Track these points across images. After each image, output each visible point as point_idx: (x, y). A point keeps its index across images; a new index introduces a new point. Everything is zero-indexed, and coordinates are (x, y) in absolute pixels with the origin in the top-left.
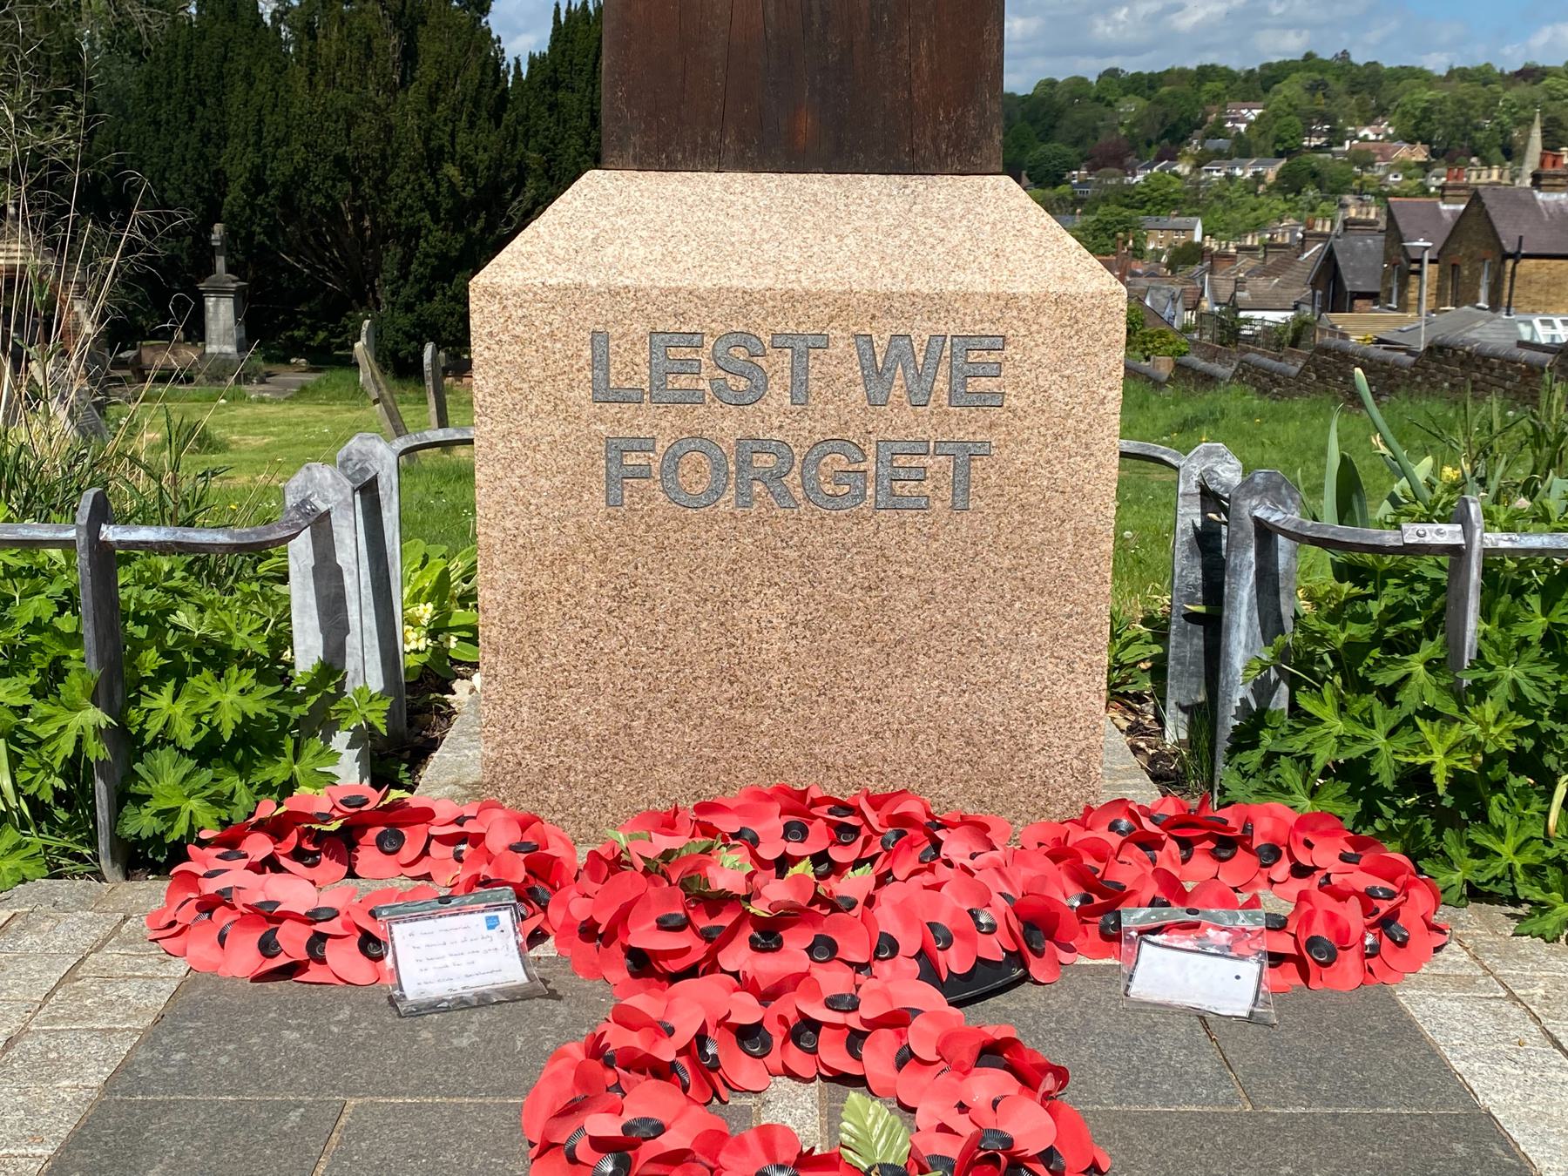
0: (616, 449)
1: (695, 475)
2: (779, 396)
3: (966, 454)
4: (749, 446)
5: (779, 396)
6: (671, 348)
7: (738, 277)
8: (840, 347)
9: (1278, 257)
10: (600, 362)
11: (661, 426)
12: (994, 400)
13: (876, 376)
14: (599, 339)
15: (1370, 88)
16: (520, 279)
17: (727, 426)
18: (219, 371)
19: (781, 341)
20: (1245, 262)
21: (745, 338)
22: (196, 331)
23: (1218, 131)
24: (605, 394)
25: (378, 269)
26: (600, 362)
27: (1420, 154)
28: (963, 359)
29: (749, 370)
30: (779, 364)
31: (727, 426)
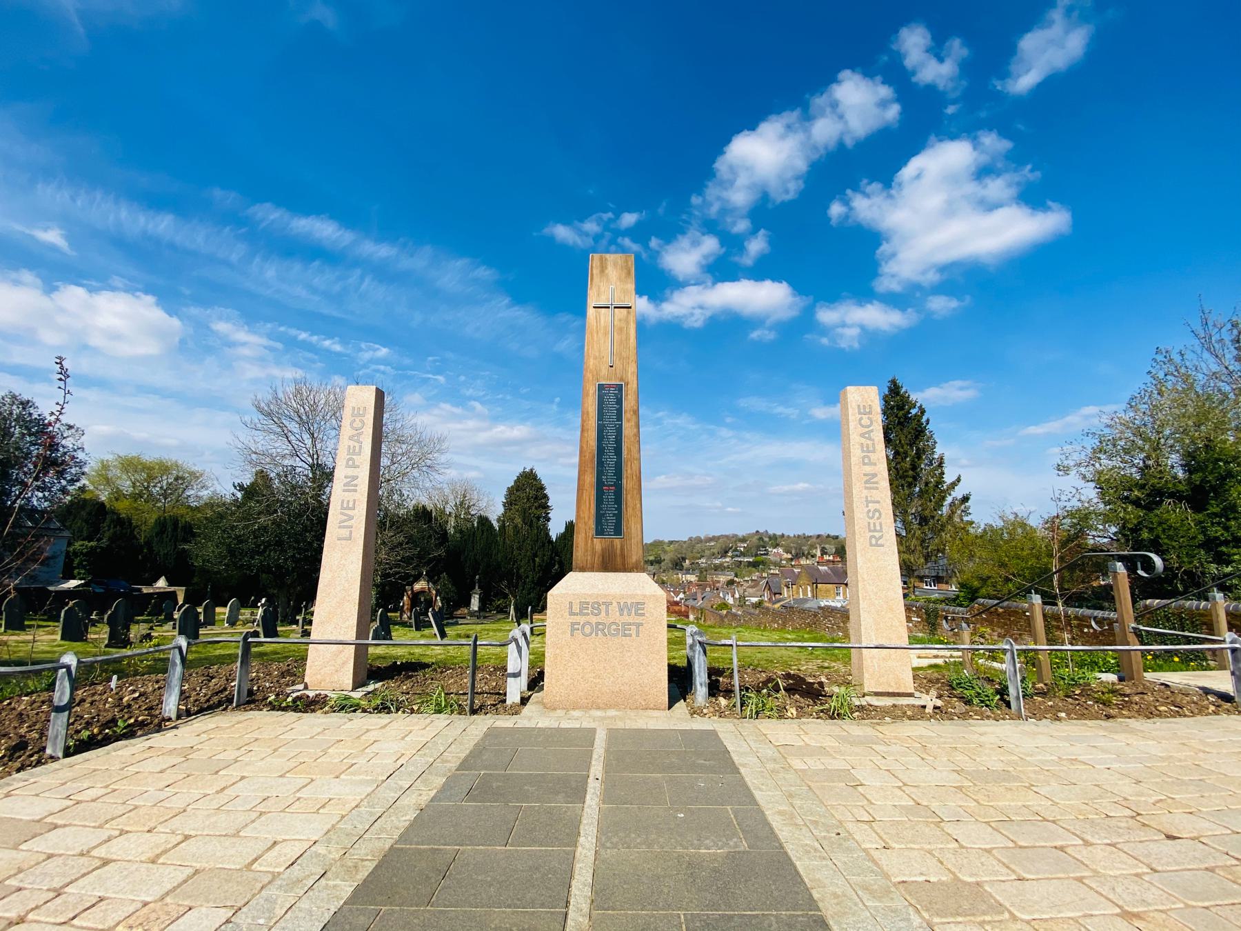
0: (573, 624)
1: (587, 630)
2: (603, 614)
3: (638, 625)
4: (598, 624)
5: (603, 614)
6: (584, 605)
7: (595, 591)
8: (615, 604)
9: (755, 583)
10: (571, 607)
11: (582, 619)
12: (643, 615)
13: (621, 610)
14: (571, 603)
15: (775, 540)
16: (558, 594)
17: (594, 620)
18: (472, 614)
19: (604, 603)
20: (746, 585)
21: (597, 603)
22: (468, 604)
23: (736, 550)
24: (572, 614)
25: (1190, 609)
26: (571, 607)
27: (789, 556)
28: (637, 607)
29: (598, 609)
30: (603, 608)
31: (594, 620)
